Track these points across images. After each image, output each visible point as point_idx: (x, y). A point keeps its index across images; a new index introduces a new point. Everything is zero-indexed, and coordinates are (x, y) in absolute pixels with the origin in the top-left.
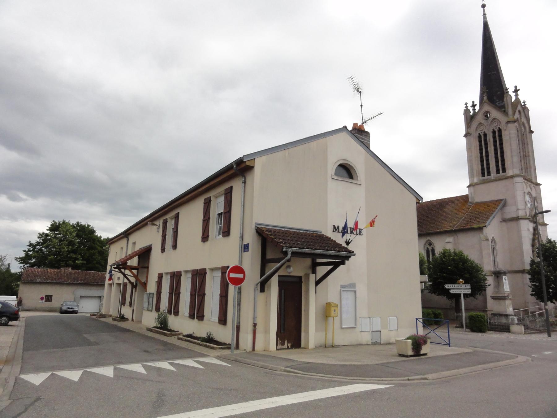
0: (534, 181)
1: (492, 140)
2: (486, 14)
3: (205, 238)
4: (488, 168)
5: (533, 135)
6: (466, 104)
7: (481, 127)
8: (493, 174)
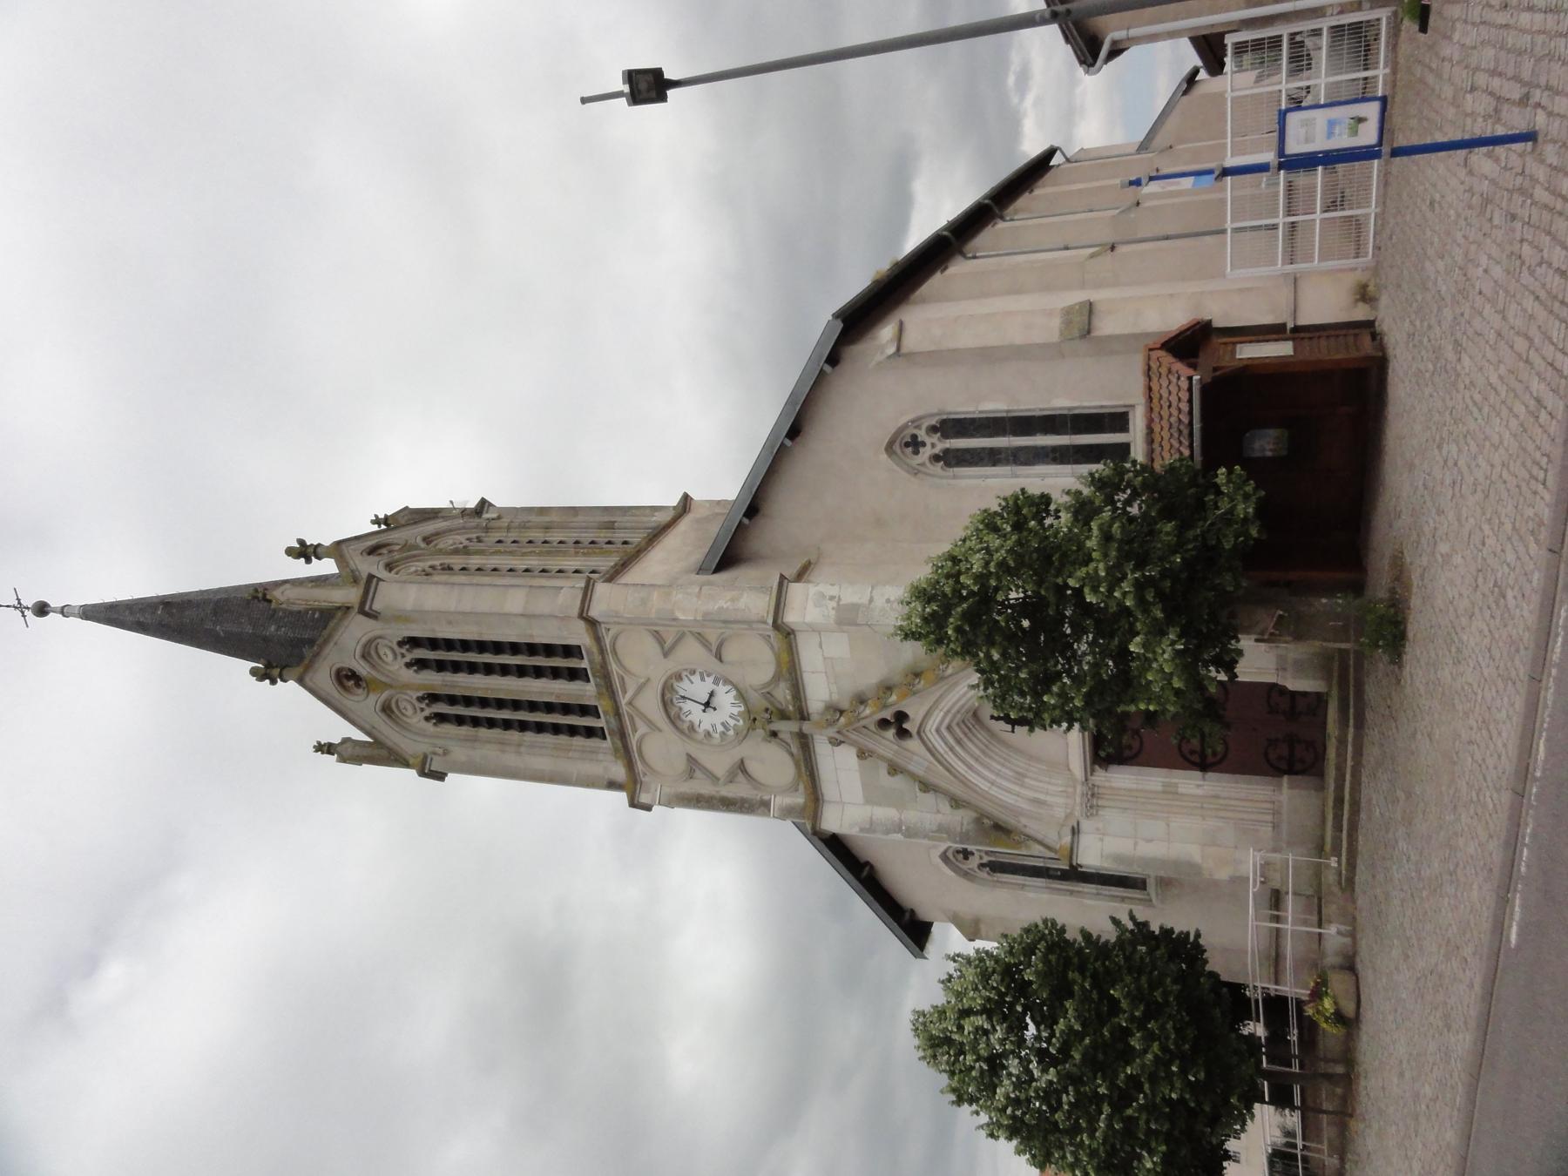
0: (663, 518)
1: (448, 677)
5: (696, 495)
6: (325, 748)
7: (402, 705)
8: (584, 692)
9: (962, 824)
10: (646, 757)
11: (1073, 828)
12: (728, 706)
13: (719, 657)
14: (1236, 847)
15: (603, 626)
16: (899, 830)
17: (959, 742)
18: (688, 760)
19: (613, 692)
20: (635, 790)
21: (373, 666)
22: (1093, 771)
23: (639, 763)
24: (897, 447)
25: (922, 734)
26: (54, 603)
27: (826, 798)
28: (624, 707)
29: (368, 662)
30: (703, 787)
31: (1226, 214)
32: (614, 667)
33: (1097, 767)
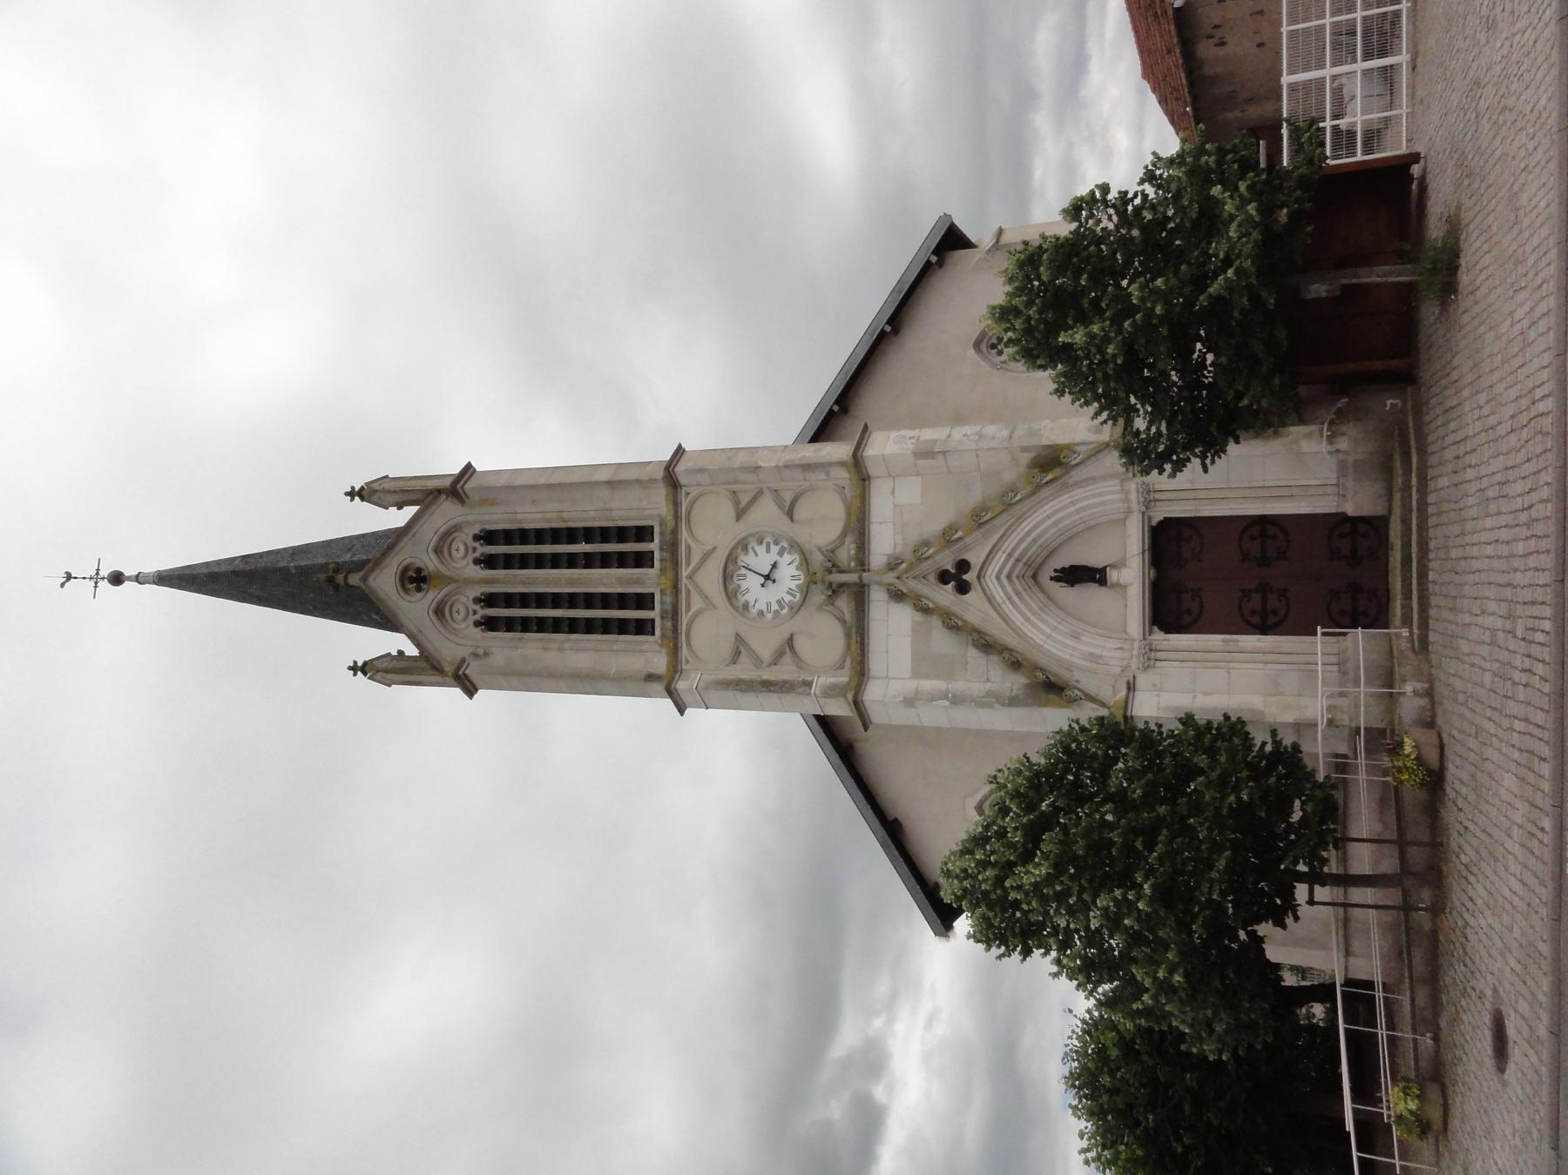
2: (140, 573)
3: (1025, 756)
4: (623, 601)
9: (1012, 690)
10: (692, 643)
11: (1128, 683)
12: (790, 575)
13: (790, 514)
14: (1300, 695)
15: (684, 489)
16: (946, 697)
17: (1018, 594)
18: (736, 638)
19: (677, 564)
20: (673, 678)
21: (442, 562)
22: (1151, 632)
23: (684, 645)
24: (983, 347)
25: (982, 580)
26: (128, 571)
27: (873, 673)
28: (684, 579)
29: (439, 557)
30: (744, 671)
31: (1281, 150)
32: (684, 535)
33: (1155, 628)
